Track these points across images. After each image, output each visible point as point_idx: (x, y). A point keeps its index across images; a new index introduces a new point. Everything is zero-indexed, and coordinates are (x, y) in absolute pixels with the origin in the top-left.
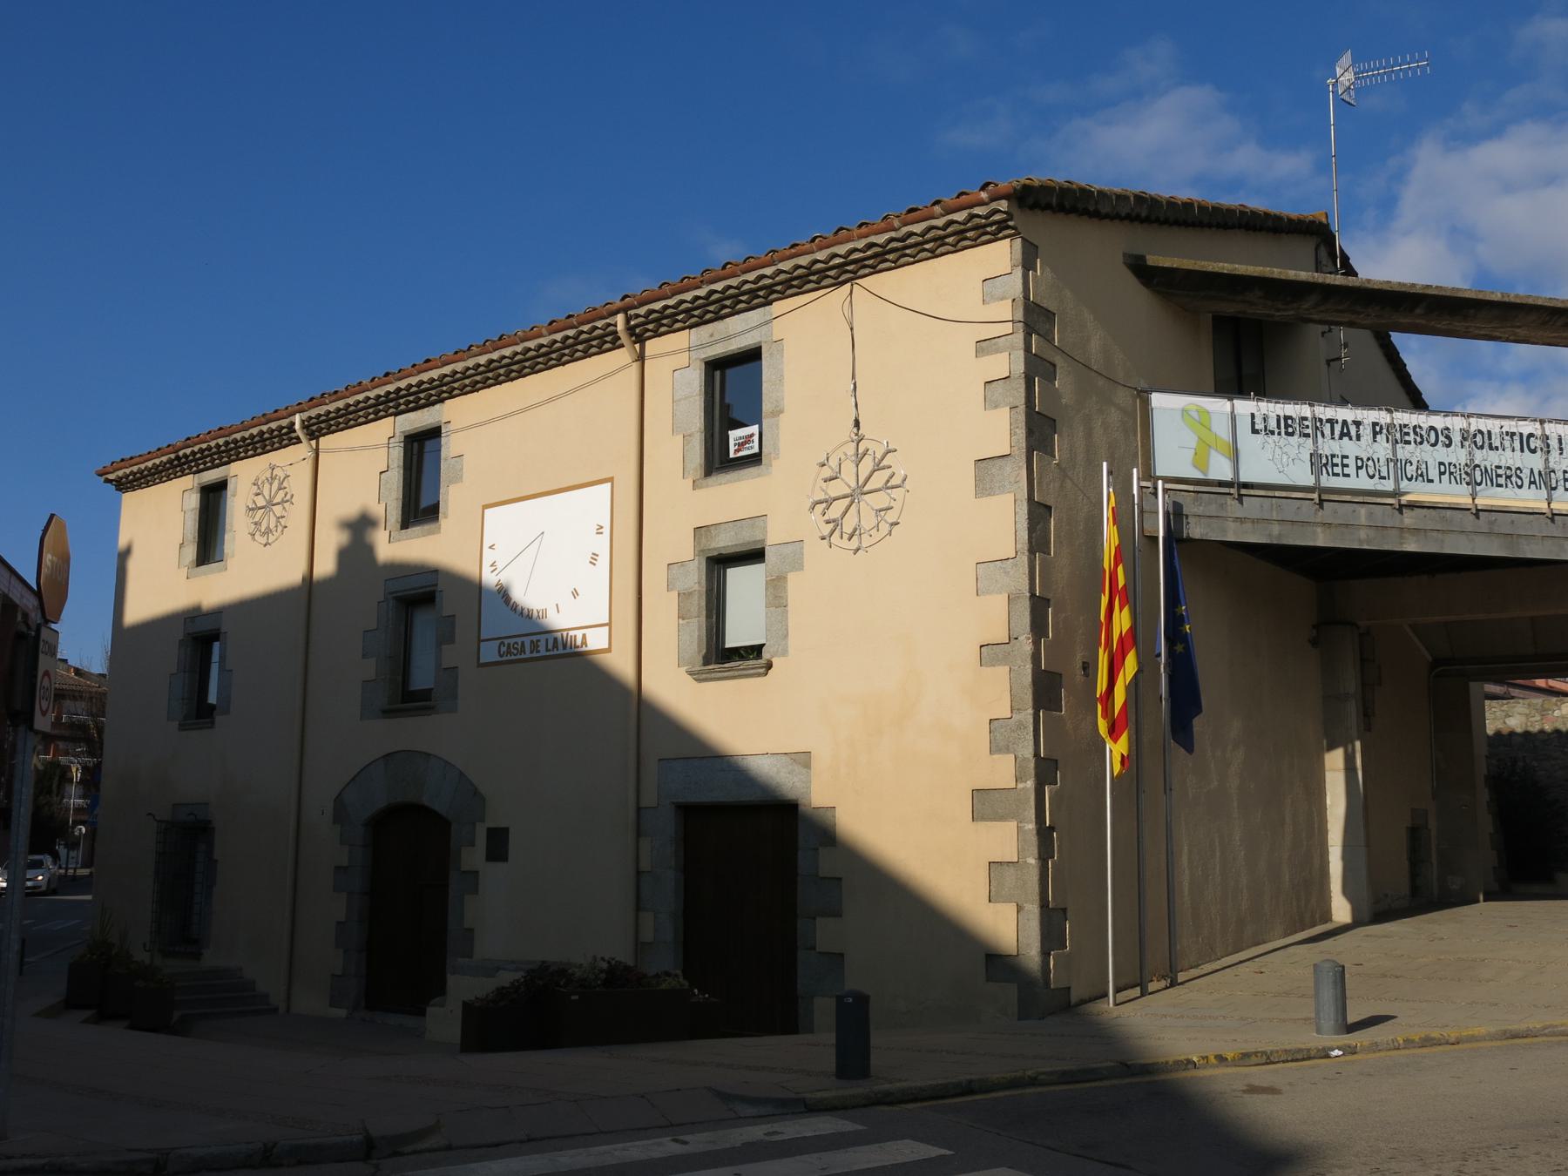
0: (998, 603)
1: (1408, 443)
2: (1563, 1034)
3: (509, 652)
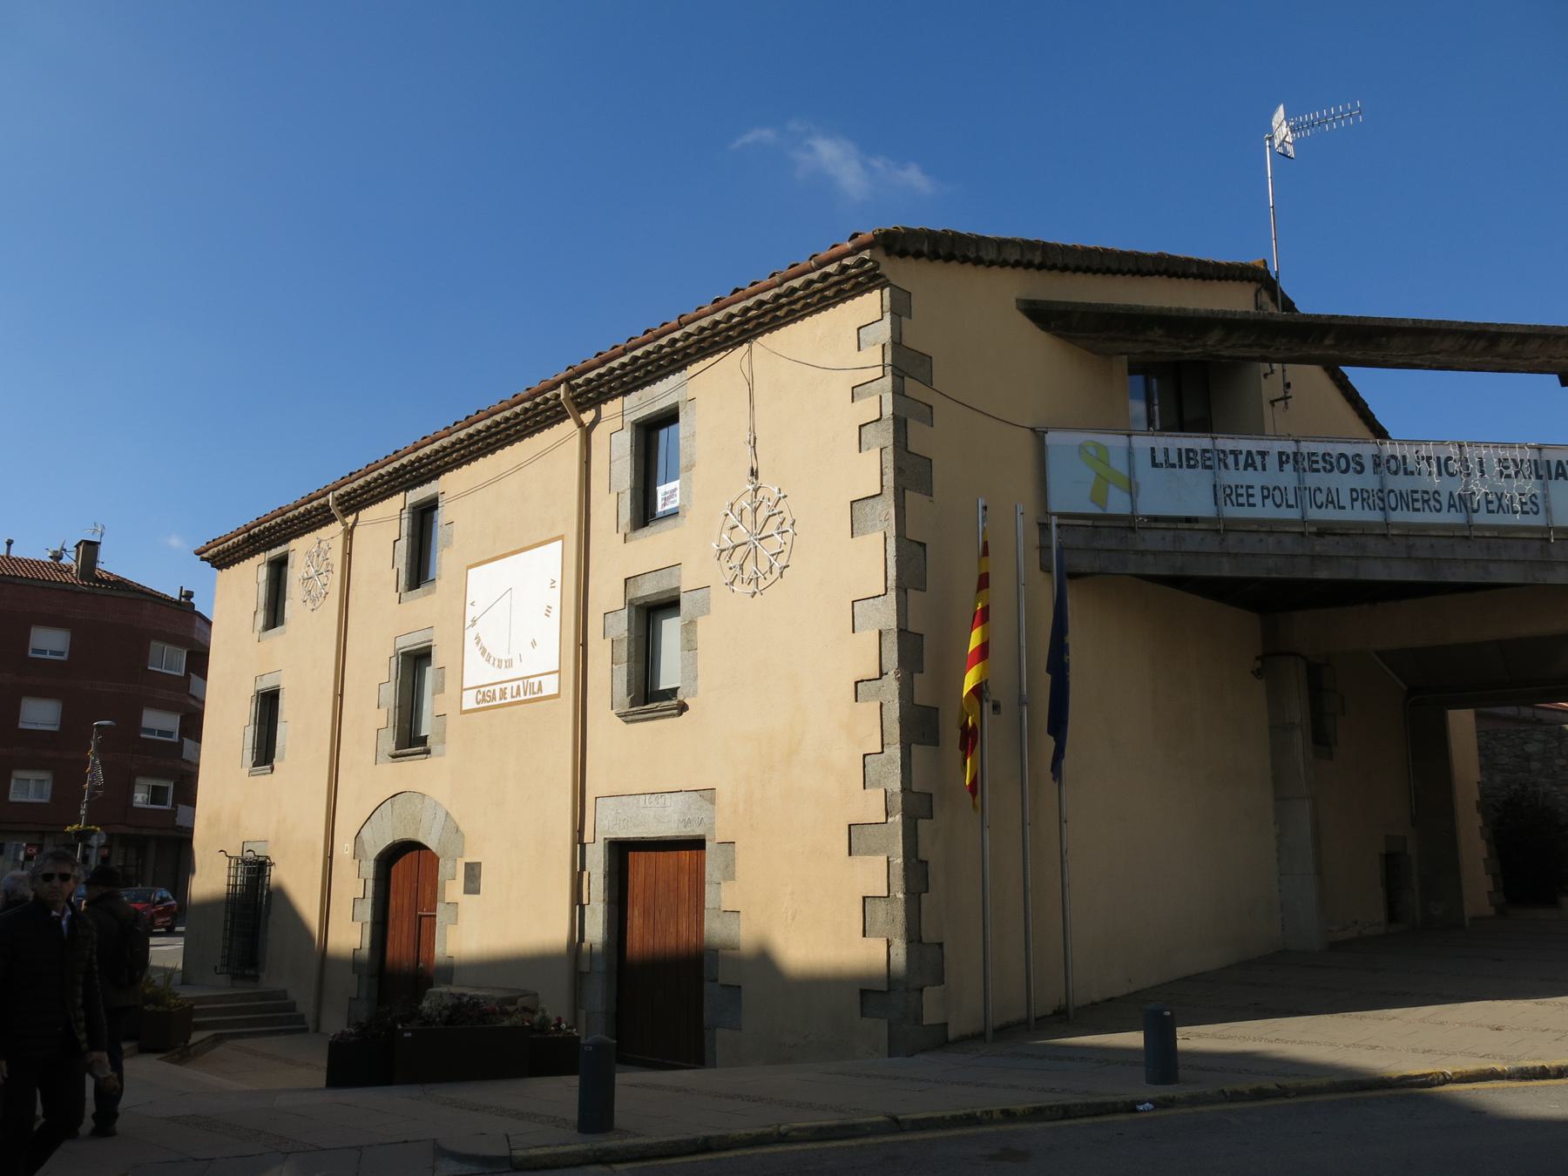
1: (1317, 470)
2: (1561, 1073)
3: (484, 700)
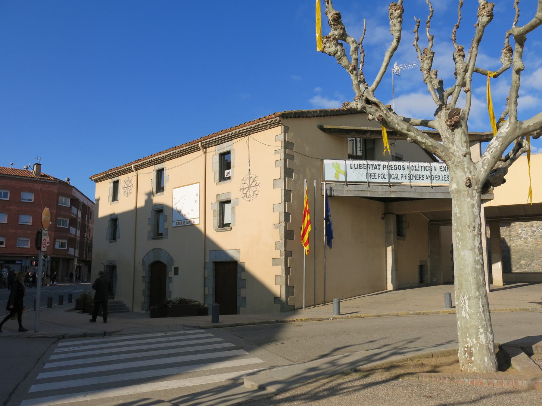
0: (278, 214)
